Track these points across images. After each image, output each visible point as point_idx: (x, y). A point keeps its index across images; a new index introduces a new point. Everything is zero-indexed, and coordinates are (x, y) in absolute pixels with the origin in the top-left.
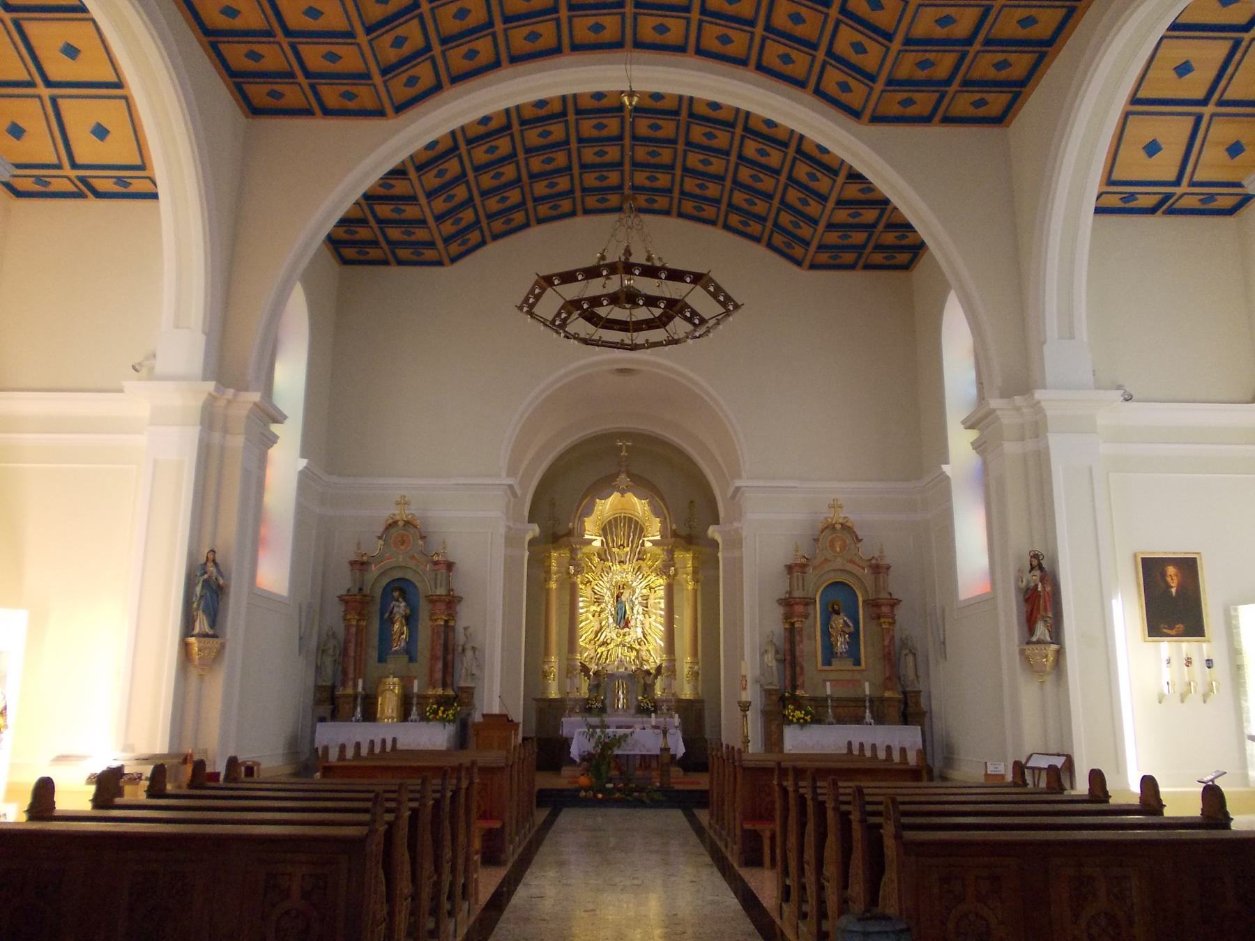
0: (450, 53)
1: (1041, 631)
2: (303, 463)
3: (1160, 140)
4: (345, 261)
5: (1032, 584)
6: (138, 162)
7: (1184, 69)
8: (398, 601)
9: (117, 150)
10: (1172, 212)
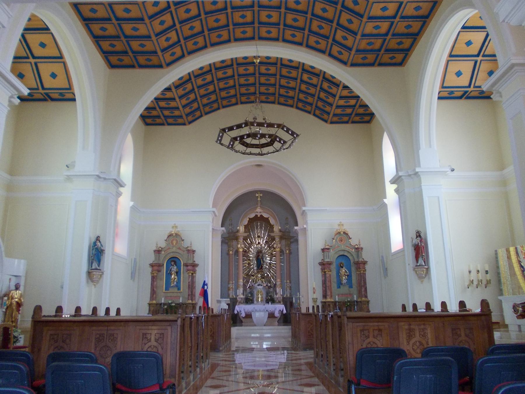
0: (188, 43)
1: (421, 261)
2: (132, 203)
3: (461, 71)
4: (147, 124)
5: (417, 243)
6: (68, 87)
7: (469, 43)
8: (173, 266)
9: (60, 82)
10: (468, 98)
